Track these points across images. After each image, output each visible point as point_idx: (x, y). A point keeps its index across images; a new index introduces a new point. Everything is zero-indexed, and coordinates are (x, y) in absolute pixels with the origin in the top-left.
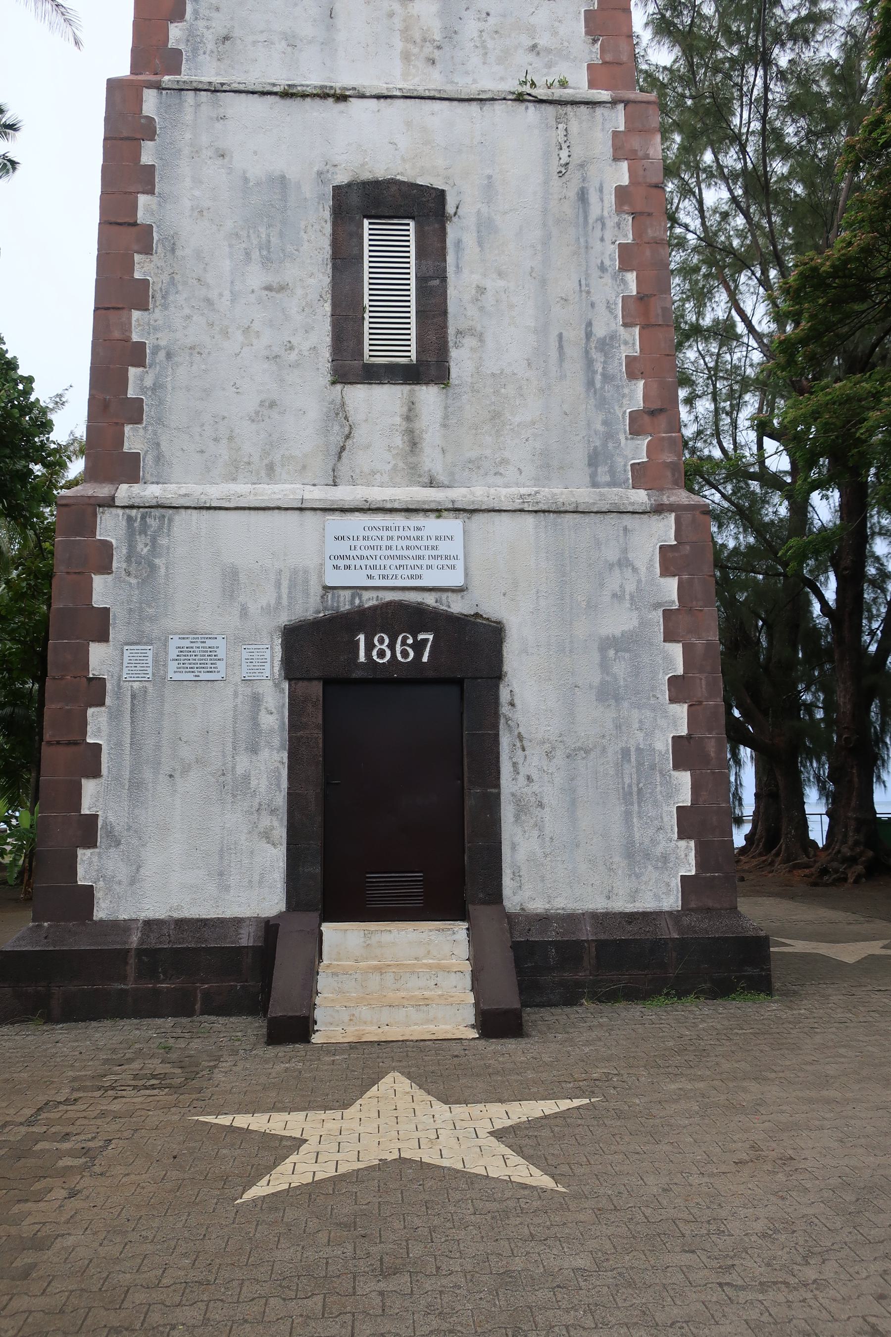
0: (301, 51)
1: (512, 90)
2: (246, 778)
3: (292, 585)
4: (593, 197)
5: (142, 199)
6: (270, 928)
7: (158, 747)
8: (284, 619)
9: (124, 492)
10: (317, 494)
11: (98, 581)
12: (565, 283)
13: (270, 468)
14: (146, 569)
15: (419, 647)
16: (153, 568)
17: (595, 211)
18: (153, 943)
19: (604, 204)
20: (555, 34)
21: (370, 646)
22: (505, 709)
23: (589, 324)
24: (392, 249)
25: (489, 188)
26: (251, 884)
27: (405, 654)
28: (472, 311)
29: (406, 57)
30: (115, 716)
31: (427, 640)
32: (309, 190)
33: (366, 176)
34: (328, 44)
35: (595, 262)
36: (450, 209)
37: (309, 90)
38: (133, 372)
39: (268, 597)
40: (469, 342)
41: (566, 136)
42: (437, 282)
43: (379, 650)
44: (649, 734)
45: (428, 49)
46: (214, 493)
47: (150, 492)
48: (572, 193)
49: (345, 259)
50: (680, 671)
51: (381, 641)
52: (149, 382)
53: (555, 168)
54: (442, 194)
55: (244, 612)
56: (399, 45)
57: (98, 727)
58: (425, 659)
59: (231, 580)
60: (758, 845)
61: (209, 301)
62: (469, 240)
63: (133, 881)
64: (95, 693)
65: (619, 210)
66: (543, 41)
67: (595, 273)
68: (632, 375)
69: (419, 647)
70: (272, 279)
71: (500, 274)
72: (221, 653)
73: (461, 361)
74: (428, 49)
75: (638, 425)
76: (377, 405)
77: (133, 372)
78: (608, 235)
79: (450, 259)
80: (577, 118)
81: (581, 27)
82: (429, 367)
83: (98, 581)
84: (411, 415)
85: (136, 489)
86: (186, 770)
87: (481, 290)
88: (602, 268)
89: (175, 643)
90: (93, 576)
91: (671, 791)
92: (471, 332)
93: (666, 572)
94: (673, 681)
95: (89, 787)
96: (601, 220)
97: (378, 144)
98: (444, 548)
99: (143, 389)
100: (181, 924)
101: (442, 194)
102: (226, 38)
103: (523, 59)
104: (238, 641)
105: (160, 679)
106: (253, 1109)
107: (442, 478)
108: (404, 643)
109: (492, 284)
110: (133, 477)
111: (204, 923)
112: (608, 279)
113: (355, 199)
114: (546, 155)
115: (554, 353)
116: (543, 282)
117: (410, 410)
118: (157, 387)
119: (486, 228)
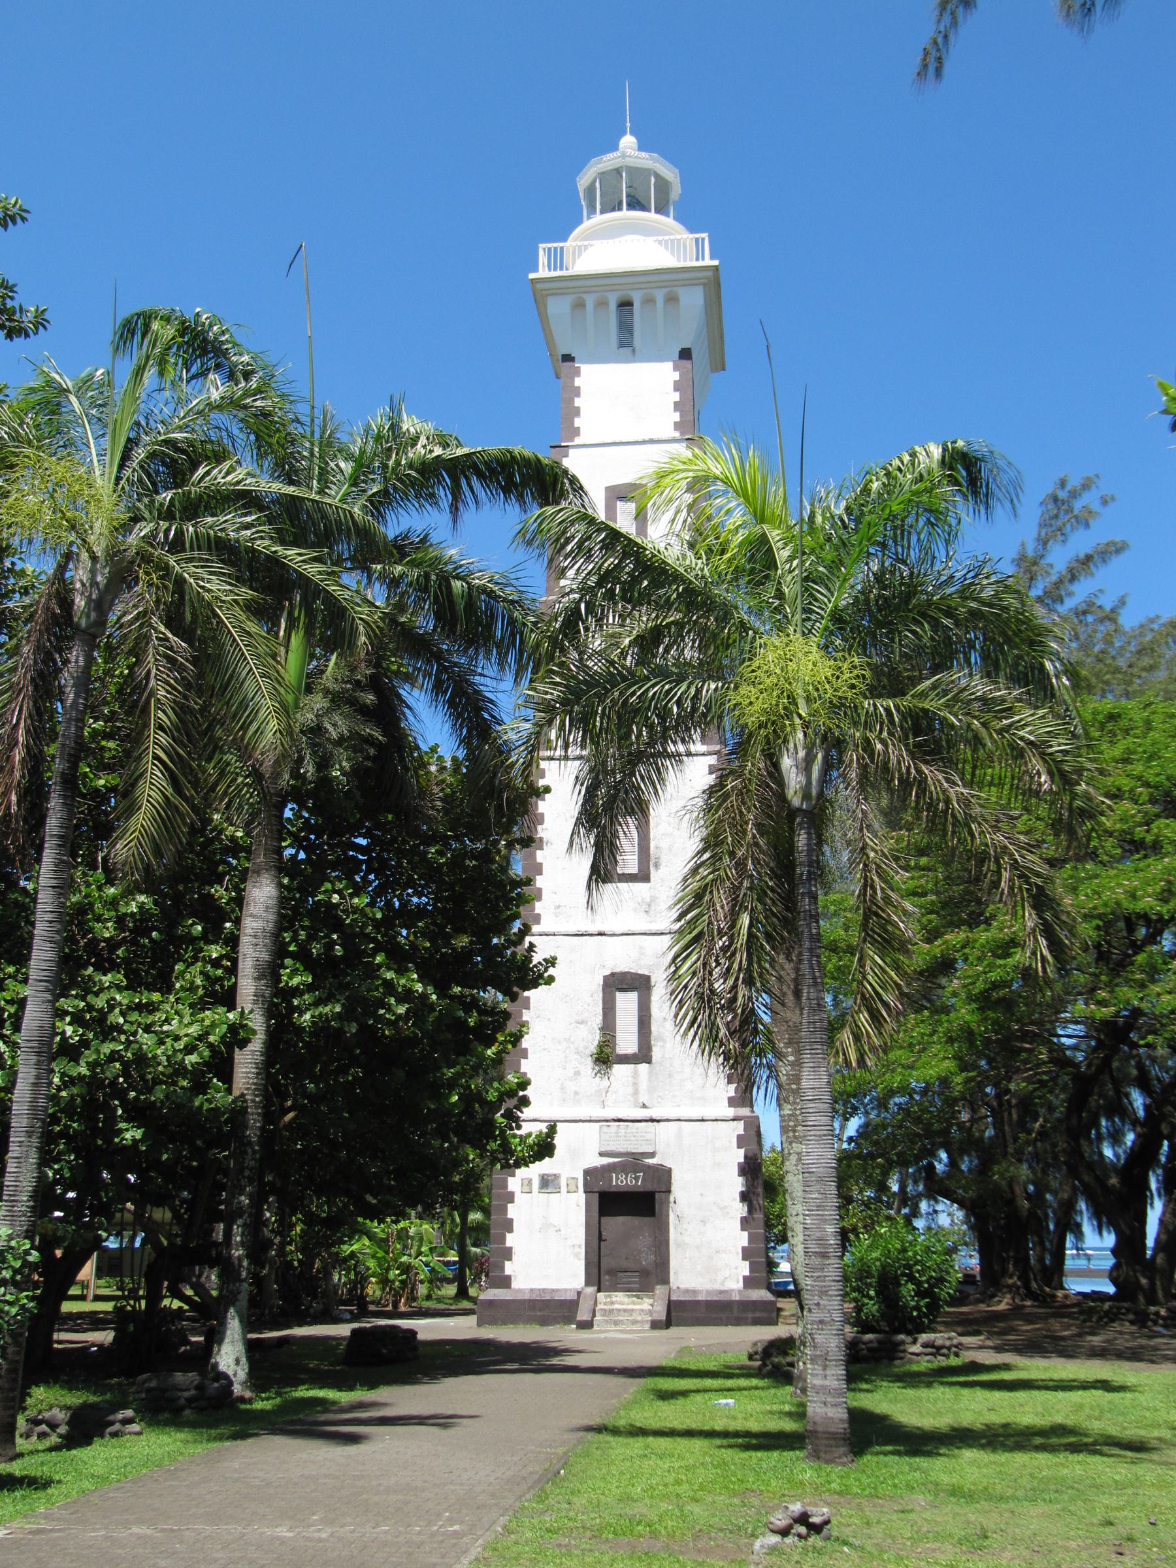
15: (636, 1179)
24: (627, 1002)
33: (617, 970)
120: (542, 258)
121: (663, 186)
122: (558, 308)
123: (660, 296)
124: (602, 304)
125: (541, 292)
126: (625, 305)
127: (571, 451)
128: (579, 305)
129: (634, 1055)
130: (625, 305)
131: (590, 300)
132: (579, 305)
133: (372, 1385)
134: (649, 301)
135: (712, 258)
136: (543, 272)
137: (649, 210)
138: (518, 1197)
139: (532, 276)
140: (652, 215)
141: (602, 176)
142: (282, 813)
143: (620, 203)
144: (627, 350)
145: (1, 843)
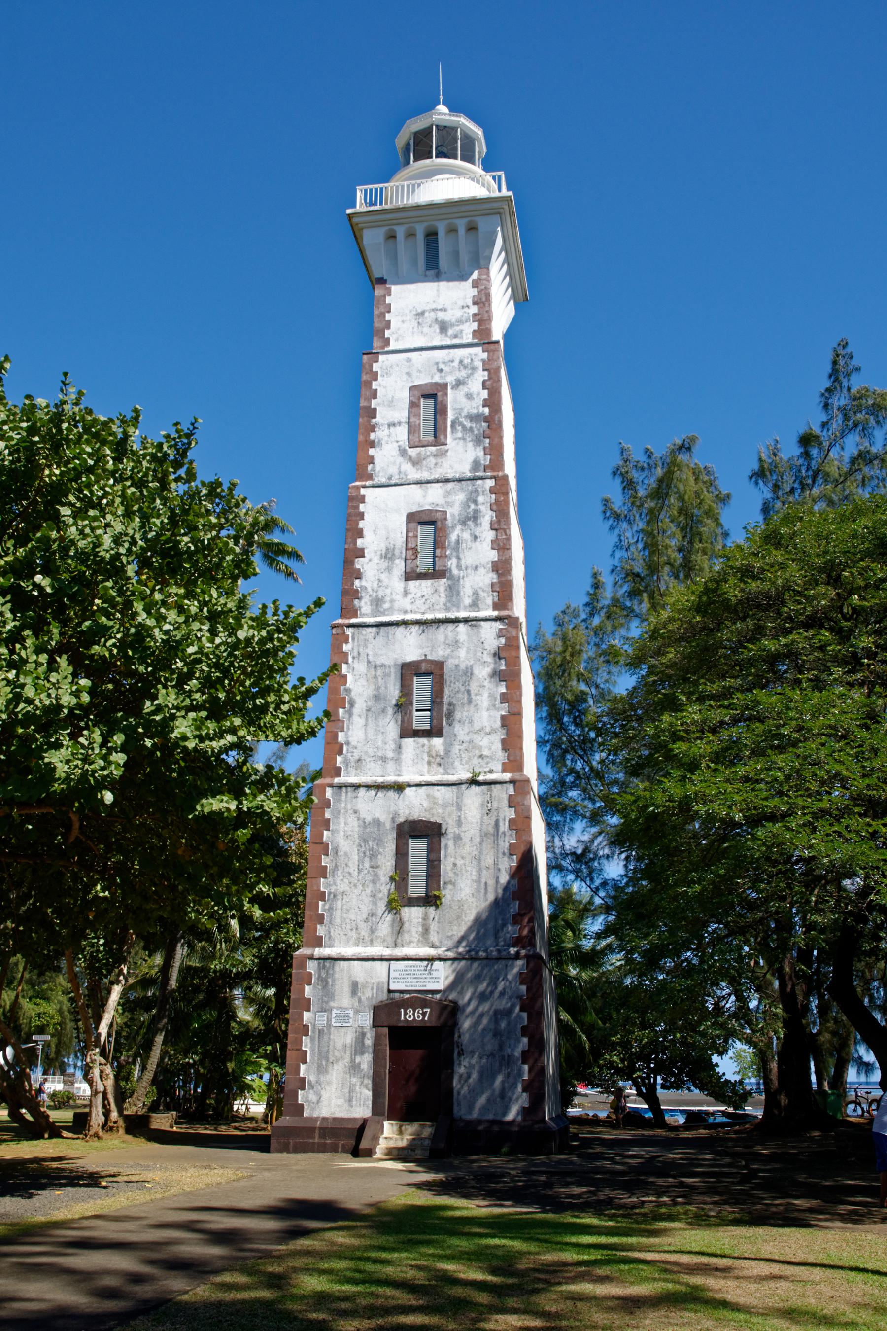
1: (96, 1143)
2: (359, 1064)
3: (378, 989)
4: (501, 824)
5: (325, 832)
6: (365, 1121)
7: (328, 1051)
8: (375, 1002)
9: (318, 952)
10: (387, 952)
12: (489, 860)
13: (372, 941)
14: (324, 982)
15: (424, 1014)
16: (327, 983)
17: (502, 829)
18: (325, 1125)
19: (504, 827)
21: (405, 1014)
23: (498, 878)
24: (417, 848)
25: (459, 823)
26: (362, 1110)
28: (451, 874)
29: (429, 763)
30: (312, 1039)
32: (388, 825)
33: (411, 818)
34: (397, 760)
35: (501, 851)
36: (443, 831)
38: (321, 903)
39: (368, 994)
40: (450, 887)
43: (411, 1016)
44: (513, 1050)
45: (438, 759)
46: (349, 952)
47: (326, 952)
48: (493, 823)
49: (401, 855)
50: (526, 1023)
51: (410, 1011)
52: (327, 907)
53: (485, 810)
54: (440, 825)
55: (360, 1000)
56: (426, 758)
57: (306, 1044)
59: (355, 988)
60: (598, 1133)
61: (350, 873)
62: (451, 844)
63: (318, 1102)
64: (305, 1030)
65: (510, 829)
66: (486, 752)
67: (500, 855)
68: (514, 899)
69: (424, 1014)
70: (704, 473)
71: (463, 858)
72: (351, 1015)
73: (447, 895)
74: (438, 759)
76: (413, 915)
77: (321, 903)
78: (507, 839)
79: (442, 853)
80: (496, 789)
81: (499, 746)
82: (431, 900)
83: (307, 988)
84: (425, 918)
85: (322, 950)
86: (337, 1061)
88: (504, 854)
89: (334, 1011)
91: (520, 1073)
92: (450, 882)
93: (522, 983)
94: (523, 1028)
95: (303, 1067)
96: (504, 833)
97: (415, 805)
99: (324, 910)
100: (335, 1119)
101: (440, 825)
102: (359, 760)
103: (475, 761)
104: (357, 1012)
105: (329, 1025)
107: (437, 943)
109: (460, 862)
111: (342, 1119)
112: (506, 859)
113: (406, 828)
114: (482, 805)
115: (483, 891)
116: (479, 861)
118: (331, 908)
119: (458, 838)
120: (359, 195)
121: (469, 142)
122: (372, 238)
123: (461, 225)
124: (411, 235)
125: (355, 227)
126: (431, 236)
127: (381, 357)
128: (392, 236)
129: (419, 898)
130: (431, 236)
131: (400, 231)
132: (392, 236)
133: (219, 1304)
134: (452, 230)
135: (508, 190)
136: (360, 206)
137: (456, 158)
138: (581, 608)
139: (349, 211)
140: (458, 162)
141: (416, 134)
142: (360, 377)
143: (430, 152)
144: (431, 273)
145: (1, 429)
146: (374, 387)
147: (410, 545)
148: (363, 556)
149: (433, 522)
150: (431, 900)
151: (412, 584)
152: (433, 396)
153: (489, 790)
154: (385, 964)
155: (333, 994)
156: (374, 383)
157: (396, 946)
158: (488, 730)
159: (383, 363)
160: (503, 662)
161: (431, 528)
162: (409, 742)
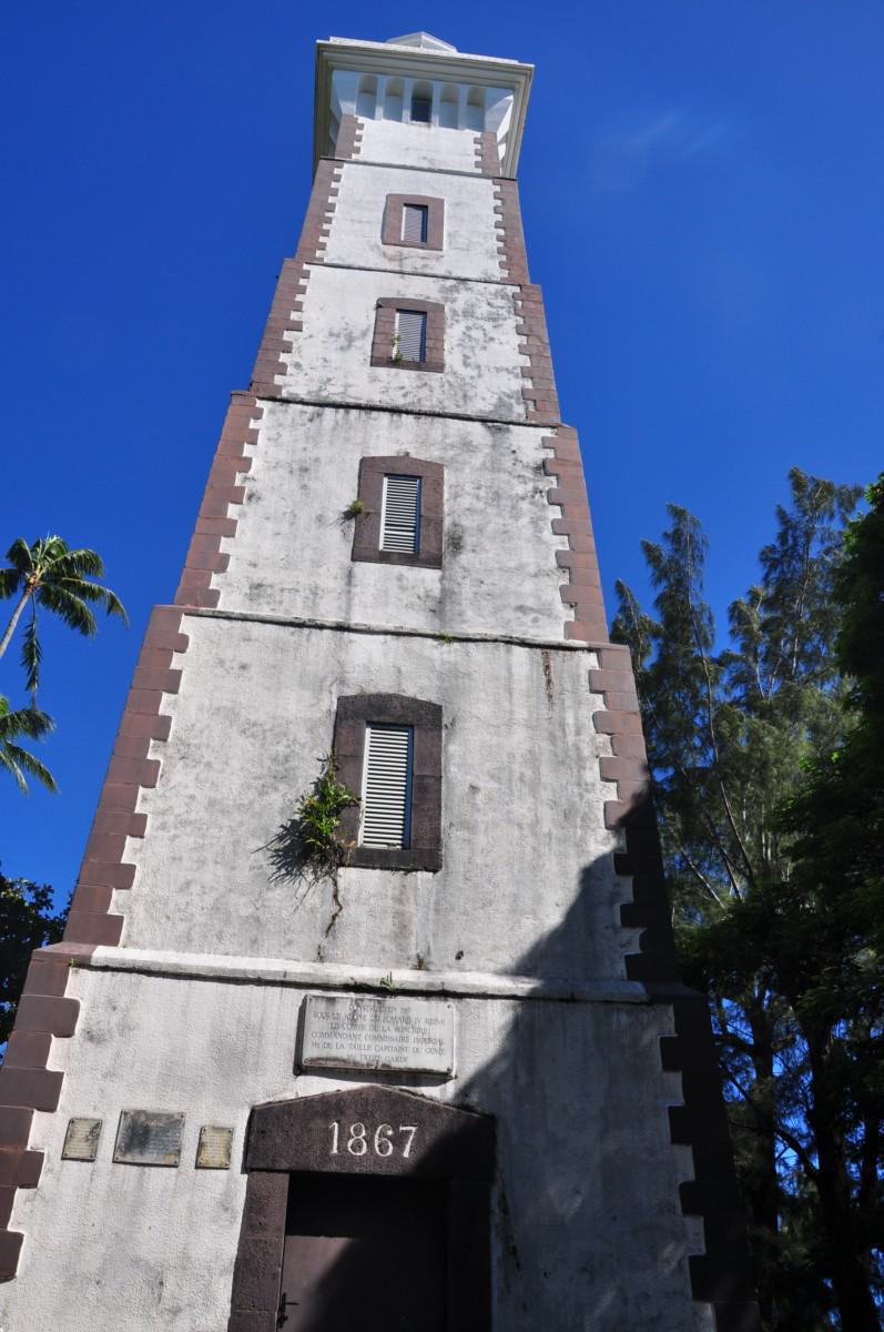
0: (322, 597)
10: (299, 968)
11: (56, 1044)
15: (398, 1141)
20: (539, 598)
22: (421, 298)
24: (381, 754)
27: (383, 1148)
31: (409, 1132)
33: (371, 690)
36: (445, 720)
37: (328, 624)
41: (69, 903)
42: (431, 781)
58: (406, 1154)
73: (455, 845)
75: (630, 917)
82: (418, 851)
87: (474, 789)
90: (53, 1036)
97: (375, 666)
98: (437, 1032)
106: (338, 1095)
108: (383, 1134)
110: (112, 939)
117: (401, 893)
123: (464, 92)
131: (383, 83)
146: (174, 665)
147: (380, 329)
148: (301, 330)
149: (424, 313)
150: (418, 851)
151: (382, 372)
152: (424, 208)
153: (547, 657)
154: (296, 996)
155: (762, 560)
156: (176, 656)
157: (321, 958)
158: (532, 569)
159: (268, 420)
160: (553, 479)
161: (418, 319)
162: (369, 572)
